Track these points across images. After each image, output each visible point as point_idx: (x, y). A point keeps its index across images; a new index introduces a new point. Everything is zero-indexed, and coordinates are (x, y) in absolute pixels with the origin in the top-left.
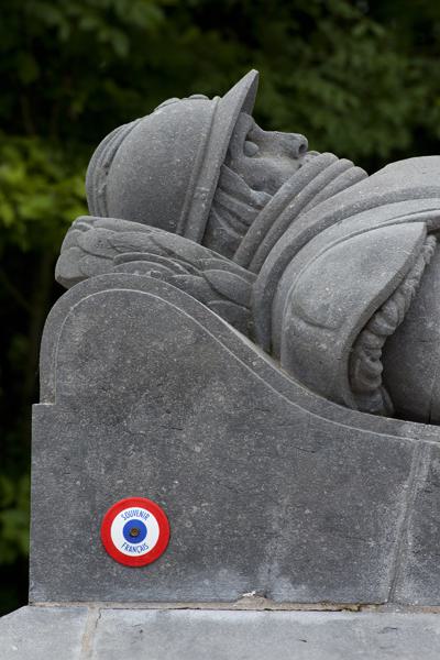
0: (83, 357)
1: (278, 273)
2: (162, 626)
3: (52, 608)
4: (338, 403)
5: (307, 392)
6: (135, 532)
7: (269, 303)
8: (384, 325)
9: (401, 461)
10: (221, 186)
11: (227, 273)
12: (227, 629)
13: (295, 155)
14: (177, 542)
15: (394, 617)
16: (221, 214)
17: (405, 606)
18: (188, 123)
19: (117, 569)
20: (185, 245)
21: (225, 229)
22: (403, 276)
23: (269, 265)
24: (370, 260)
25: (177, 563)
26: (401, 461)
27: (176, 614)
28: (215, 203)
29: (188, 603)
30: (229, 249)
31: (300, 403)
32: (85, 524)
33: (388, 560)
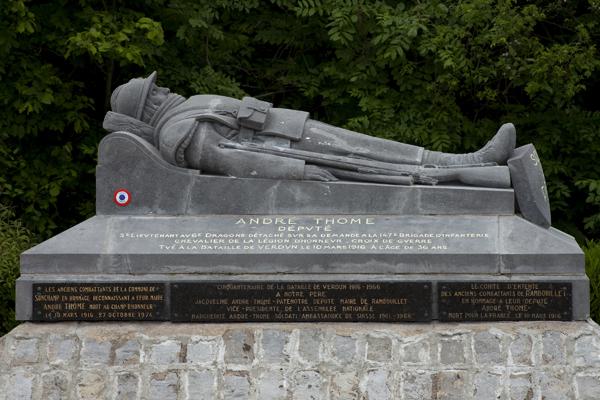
0: (108, 154)
1: (160, 128)
2: (129, 220)
3: (102, 216)
4: (408, 143)
5: (165, 162)
6: (122, 198)
7: (158, 136)
8: (184, 146)
9: (188, 179)
10: (146, 104)
11: (147, 128)
12: (145, 221)
13: (166, 94)
14: (133, 200)
15: (187, 218)
16: (147, 115)
17: (189, 215)
18: (138, 85)
19: (120, 208)
20: (136, 121)
21: (147, 116)
22: (188, 134)
23: (158, 125)
24: (181, 128)
25: (133, 205)
26: (188, 179)
27: (133, 217)
28: (144, 108)
29: (136, 215)
30: (148, 122)
31: (163, 165)
32: (110, 196)
33: (185, 204)
